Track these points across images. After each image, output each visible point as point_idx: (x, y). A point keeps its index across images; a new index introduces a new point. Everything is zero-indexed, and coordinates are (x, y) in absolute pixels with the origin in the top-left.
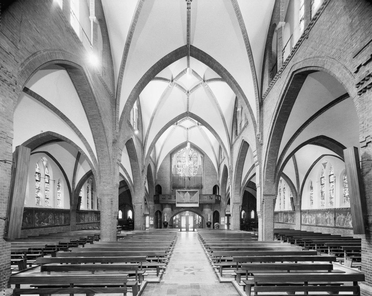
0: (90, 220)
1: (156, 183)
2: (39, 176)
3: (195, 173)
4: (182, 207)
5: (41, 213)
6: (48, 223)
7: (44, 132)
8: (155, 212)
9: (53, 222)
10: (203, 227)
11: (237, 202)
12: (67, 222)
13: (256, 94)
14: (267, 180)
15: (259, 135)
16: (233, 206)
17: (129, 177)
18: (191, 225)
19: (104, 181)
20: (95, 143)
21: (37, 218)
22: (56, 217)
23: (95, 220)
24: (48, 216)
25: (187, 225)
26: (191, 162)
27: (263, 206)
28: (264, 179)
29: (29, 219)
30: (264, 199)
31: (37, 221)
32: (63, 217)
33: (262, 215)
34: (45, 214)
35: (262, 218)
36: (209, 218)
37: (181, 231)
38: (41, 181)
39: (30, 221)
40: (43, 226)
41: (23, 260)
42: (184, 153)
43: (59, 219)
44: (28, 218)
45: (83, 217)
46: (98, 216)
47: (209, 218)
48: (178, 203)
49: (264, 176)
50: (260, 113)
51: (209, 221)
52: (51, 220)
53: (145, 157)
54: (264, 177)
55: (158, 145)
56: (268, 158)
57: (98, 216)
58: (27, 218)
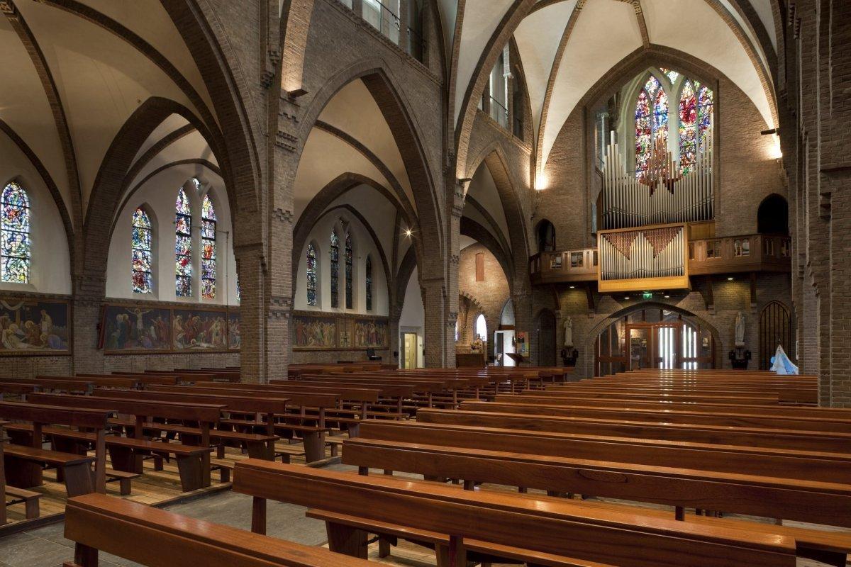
0: (342, 340)
1: (534, 216)
2: (188, 225)
5: (190, 316)
6: (208, 341)
7: (143, 101)
9: (224, 342)
10: (717, 364)
21: (180, 328)
22: (231, 328)
23: (357, 340)
26: (690, 127)
27: (826, 231)
29: (158, 329)
30: (827, 195)
31: (180, 336)
34: (202, 319)
36: (740, 334)
38: (193, 235)
39: (162, 336)
41: (264, 441)
42: (663, 100)
44: (155, 327)
45: (318, 330)
46: (369, 332)
49: (824, 70)
51: (740, 343)
52: (217, 335)
57: (369, 332)
58: (153, 328)
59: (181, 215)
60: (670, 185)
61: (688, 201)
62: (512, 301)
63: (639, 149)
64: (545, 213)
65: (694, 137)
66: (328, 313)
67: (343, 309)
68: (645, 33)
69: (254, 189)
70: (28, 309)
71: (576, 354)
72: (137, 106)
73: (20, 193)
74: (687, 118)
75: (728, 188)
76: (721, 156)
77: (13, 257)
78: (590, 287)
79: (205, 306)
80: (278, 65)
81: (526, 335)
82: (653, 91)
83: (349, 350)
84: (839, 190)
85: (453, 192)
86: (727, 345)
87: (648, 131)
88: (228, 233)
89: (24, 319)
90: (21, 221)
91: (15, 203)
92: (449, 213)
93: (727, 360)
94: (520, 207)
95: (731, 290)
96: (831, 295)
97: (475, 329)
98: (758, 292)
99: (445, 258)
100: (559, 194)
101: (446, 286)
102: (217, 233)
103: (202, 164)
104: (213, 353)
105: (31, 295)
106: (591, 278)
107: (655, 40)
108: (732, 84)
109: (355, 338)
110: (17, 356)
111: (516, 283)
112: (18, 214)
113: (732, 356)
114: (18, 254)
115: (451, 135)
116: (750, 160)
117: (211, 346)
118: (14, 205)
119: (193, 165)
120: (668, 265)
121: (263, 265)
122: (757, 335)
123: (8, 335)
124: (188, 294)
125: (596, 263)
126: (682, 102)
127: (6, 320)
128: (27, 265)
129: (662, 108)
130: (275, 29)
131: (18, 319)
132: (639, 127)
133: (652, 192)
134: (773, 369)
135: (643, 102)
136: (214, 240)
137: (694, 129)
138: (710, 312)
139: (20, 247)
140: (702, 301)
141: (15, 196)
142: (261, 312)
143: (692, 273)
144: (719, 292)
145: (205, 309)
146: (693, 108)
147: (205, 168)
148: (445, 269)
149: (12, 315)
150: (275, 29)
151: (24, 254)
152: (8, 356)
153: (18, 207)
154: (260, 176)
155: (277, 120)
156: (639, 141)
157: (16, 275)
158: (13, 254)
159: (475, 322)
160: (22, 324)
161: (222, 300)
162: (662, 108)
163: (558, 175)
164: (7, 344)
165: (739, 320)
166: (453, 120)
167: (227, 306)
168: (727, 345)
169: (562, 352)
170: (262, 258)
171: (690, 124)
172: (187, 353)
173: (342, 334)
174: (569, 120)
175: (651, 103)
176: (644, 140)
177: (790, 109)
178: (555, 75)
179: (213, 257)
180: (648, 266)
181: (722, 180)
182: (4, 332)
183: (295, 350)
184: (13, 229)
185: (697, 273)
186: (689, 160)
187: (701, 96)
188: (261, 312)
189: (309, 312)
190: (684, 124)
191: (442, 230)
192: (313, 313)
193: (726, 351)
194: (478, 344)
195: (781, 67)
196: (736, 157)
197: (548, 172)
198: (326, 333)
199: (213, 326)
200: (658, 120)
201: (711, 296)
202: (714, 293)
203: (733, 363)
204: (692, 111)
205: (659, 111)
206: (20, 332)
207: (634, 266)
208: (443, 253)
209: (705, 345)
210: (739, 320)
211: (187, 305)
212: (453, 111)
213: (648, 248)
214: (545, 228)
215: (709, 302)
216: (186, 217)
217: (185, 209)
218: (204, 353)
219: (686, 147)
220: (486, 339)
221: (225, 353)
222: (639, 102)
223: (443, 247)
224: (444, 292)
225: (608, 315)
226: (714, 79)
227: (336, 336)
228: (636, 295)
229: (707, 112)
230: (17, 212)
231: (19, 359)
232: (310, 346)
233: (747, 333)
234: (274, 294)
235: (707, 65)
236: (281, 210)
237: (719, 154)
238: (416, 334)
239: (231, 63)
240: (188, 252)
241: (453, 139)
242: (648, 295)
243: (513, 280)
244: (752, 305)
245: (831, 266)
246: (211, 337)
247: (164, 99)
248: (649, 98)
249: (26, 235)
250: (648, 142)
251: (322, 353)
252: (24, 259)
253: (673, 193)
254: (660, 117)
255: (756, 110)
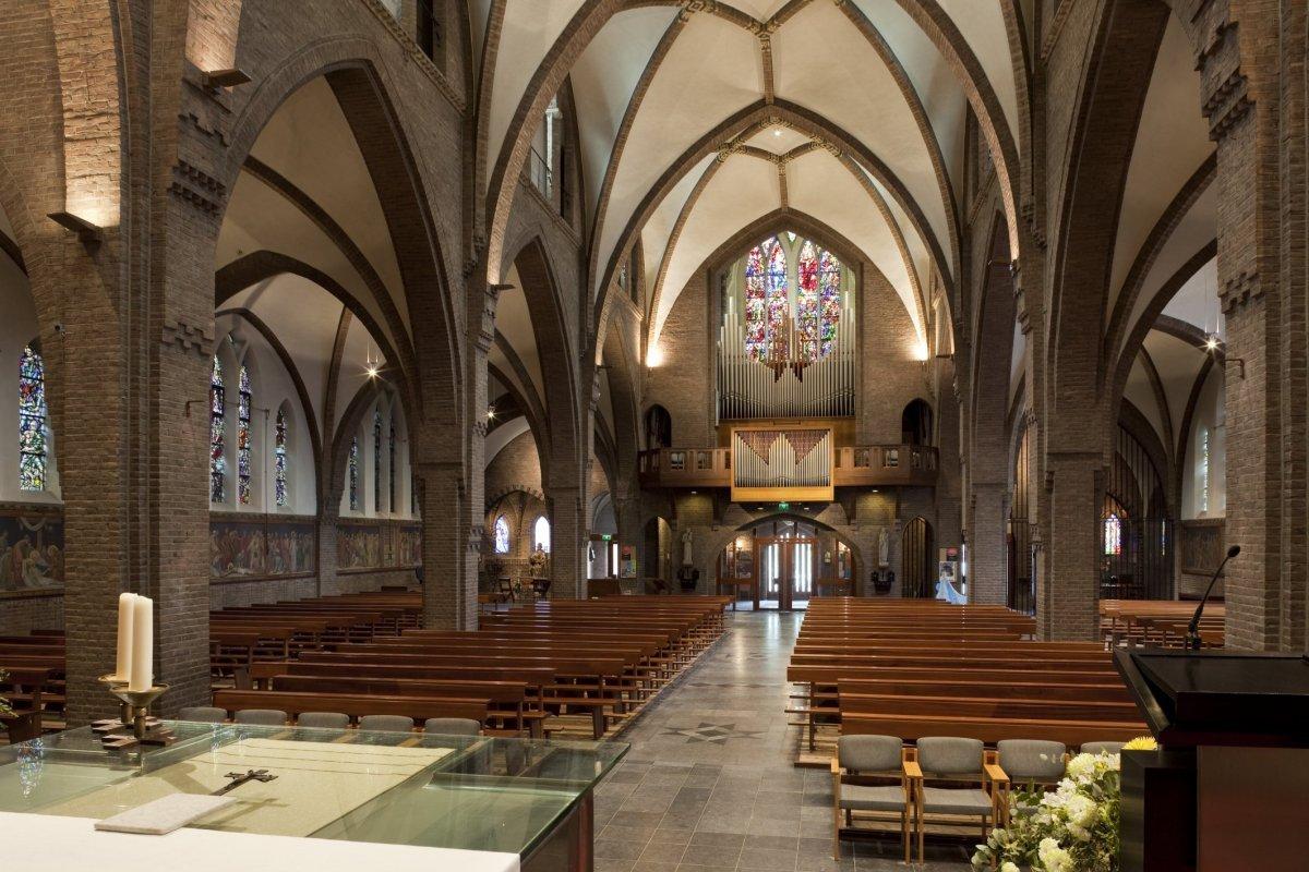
3: (826, 346)
4: (761, 504)
6: (246, 566)
7: (247, 252)
8: (643, 525)
9: (263, 565)
10: (858, 591)
11: (988, 479)
12: (306, 565)
13: (1012, 43)
14: (1067, 393)
15: (1031, 209)
16: (974, 496)
17: (528, 385)
18: (803, 578)
19: (433, 416)
20: (404, 283)
24: (247, 543)
25: (786, 578)
26: (810, 296)
28: (1051, 387)
30: (1051, 473)
32: (294, 547)
33: (1047, 536)
35: (1048, 552)
36: (884, 552)
37: (757, 608)
40: (231, 576)
42: (780, 257)
43: (281, 555)
45: (361, 544)
47: (884, 552)
48: (740, 484)
49: (1051, 375)
50: (1032, 117)
51: (883, 563)
52: (256, 555)
53: (592, 298)
54: (1051, 380)
55: (652, 235)
56: (1064, 302)
57: (414, 544)
59: (214, 387)
60: (798, 369)
61: (817, 391)
62: (615, 506)
63: (750, 315)
64: (660, 397)
65: (814, 308)
66: (372, 520)
67: (387, 515)
68: (784, 196)
69: (453, 398)
70: (51, 528)
71: (696, 575)
72: (234, 257)
73: (35, 360)
74: (807, 284)
75: (872, 387)
76: (865, 350)
77: (27, 453)
78: (720, 495)
79: (243, 515)
80: (483, 253)
81: (633, 551)
82: (768, 246)
83: (393, 570)
84: (1060, 470)
85: (591, 381)
86: (870, 565)
87: (762, 295)
88: (267, 411)
89: (46, 544)
90: (36, 400)
91: (30, 374)
92: (586, 408)
93: (869, 583)
94: (632, 388)
95: (874, 503)
96: (1053, 552)
97: (532, 537)
98: (903, 506)
99: (581, 462)
100: (676, 375)
101: (581, 496)
102: (227, 405)
103: (241, 314)
104: (254, 581)
105: (55, 508)
106: (722, 484)
107: (794, 204)
108: (877, 271)
109: (401, 553)
110: (37, 597)
111: (619, 483)
112: (32, 390)
113: (875, 578)
114: (33, 448)
115: (590, 311)
116: (895, 359)
117: (250, 572)
118: (28, 378)
119: (230, 316)
120: (812, 475)
121: (461, 488)
122: (900, 554)
123: (28, 567)
124: (221, 497)
125: (728, 465)
126: (801, 264)
127: (26, 545)
128: (43, 464)
129: (779, 268)
130: (481, 211)
131: (39, 543)
132: (750, 287)
133: (777, 379)
134: (938, 597)
135: (755, 257)
136: (248, 421)
137: (814, 298)
138: (852, 527)
139: (35, 438)
140: (844, 514)
141: (30, 364)
142: (458, 544)
143: (838, 484)
144: (861, 505)
145: (243, 520)
146: (814, 273)
147: (244, 321)
148: (581, 476)
149: (33, 535)
150: (481, 211)
151: (39, 448)
152: (28, 598)
153: (33, 379)
154: (459, 382)
155: (480, 317)
156: (750, 305)
157: (30, 478)
158: (26, 449)
159: (533, 527)
160: (44, 551)
161: (260, 507)
162: (779, 268)
163: (676, 351)
164: (28, 581)
165: (882, 537)
166: (593, 293)
167: (266, 515)
168: (870, 565)
169: (678, 573)
170: (461, 480)
171: (811, 292)
172: (223, 583)
173: (386, 547)
174: (692, 282)
175: (766, 260)
176: (756, 304)
177: (965, 340)
178: (680, 230)
179: (246, 445)
180: (790, 474)
181: (865, 378)
182: (25, 562)
183: (340, 574)
184: (27, 413)
185: (843, 484)
186: (809, 336)
187: (823, 260)
188: (458, 544)
189: (352, 519)
190: (803, 291)
191: (577, 427)
192: (357, 520)
193: (868, 572)
194: (539, 557)
195: (958, 294)
196: (880, 353)
197: (663, 345)
198: (370, 547)
199: (252, 544)
200: (773, 282)
201: (854, 508)
202: (857, 505)
203: (876, 586)
204: (813, 277)
205: (775, 271)
206: (43, 563)
207: (773, 472)
208: (578, 457)
209: (828, 561)
210: (882, 537)
211: (224, 515)
212: (594, 282)
213: (790, 451)
214: (660, 420)
215: (850, 517)
216: (218, 388)
217: (217, 377)
218: (242, 582)
219: (805, 319)
220: (548, 551)
221: (264, 580)
222: (751, 257)
223: (578, 449)
224: (579, 504)
225: (736, 528)
226: (858, 260)
227: (380, 552)
228: (771, 506)
229: (829, 280)
230: (31, 388)
231: (40, 601)
232: (353, 568)
233: (891, 552)
234: (474, 523)
235: (851, 245)
236: (185, 326)
237: (862, 348)
238: (814, 592)
239: (444, 251)
240: (220, 439)
241: (592, 316)
242: (784, 506)
243: (615, 479)
244: (897, 521)
245: (1053, 529)
246: (248, 561)
247: (288, 258)
248: (763, 254)
249: (42, 420)
250: (761, 308)
251: (367, 575)
252: (39, 456)
253: (801, 381)
254: (776, 279)
255: (902, 305)
